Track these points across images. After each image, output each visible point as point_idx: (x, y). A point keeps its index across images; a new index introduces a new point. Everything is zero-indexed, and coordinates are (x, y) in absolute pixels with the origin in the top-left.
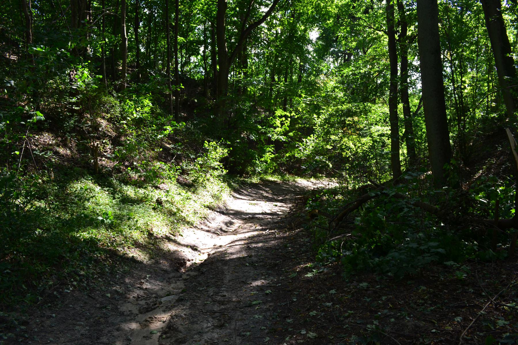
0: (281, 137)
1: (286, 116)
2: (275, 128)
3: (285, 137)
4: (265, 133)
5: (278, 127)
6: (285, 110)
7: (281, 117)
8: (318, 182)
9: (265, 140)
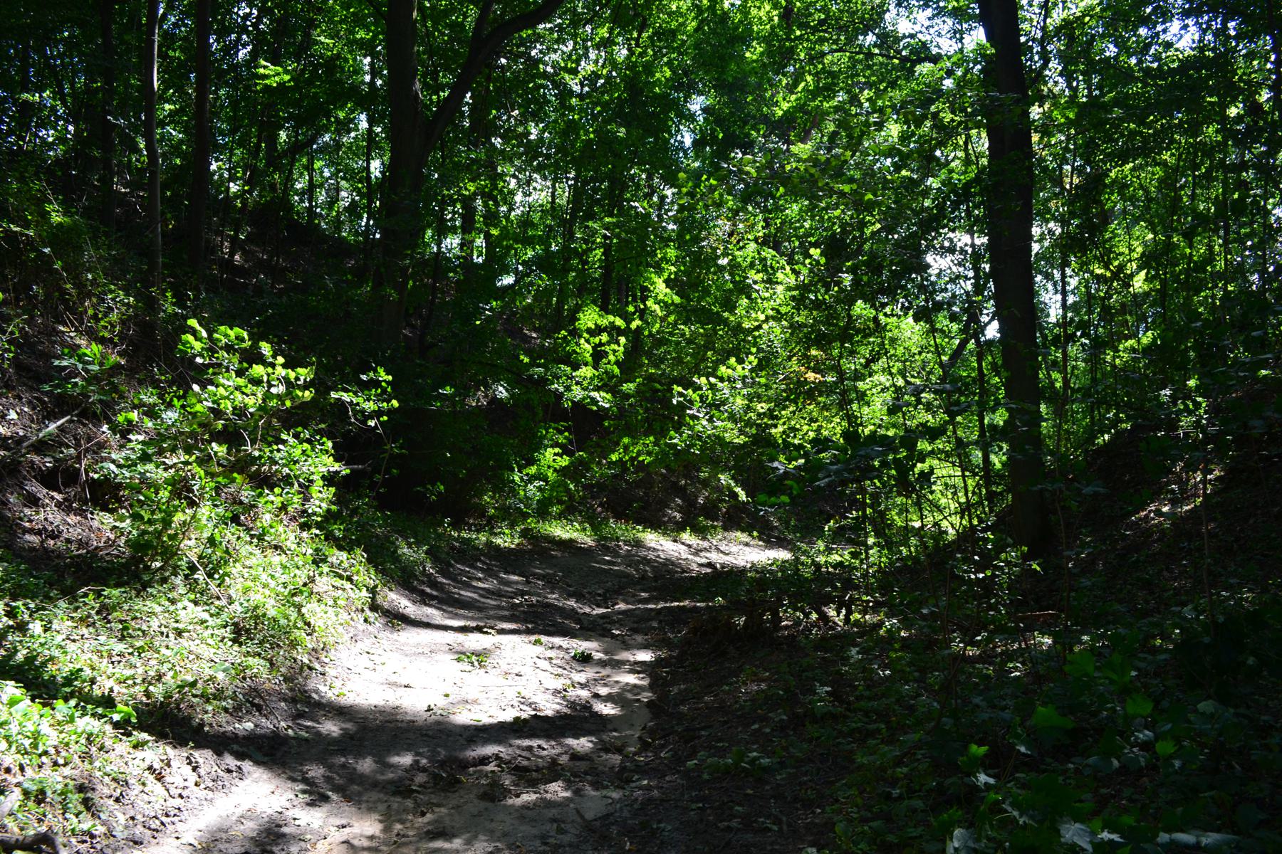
0: (595, 394)
1: (614, 331)
2: (576, 367)
3: (609, 396)
4: (543, 381)
5: (586, 364)
6: (605, 309)
7: (598, 330)
8: (705, 544)
9: (546, 407)
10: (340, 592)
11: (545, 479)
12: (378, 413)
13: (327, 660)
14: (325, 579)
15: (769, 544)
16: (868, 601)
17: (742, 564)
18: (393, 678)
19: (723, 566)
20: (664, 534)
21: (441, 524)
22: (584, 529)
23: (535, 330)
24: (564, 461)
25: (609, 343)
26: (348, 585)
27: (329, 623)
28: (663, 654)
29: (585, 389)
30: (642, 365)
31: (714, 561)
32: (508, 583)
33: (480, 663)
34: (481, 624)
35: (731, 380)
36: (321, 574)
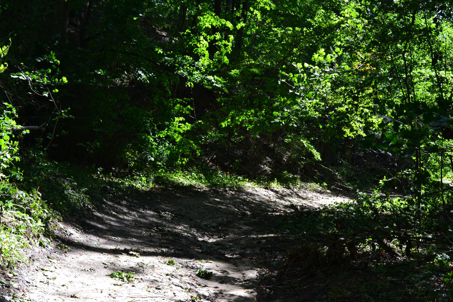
1: (225, 31)
6: (218, 12)
7: (213, 30)
9: (173, 87)
10: (21, 222)
11: (173, 141)
12: (49, 87)
13: (11, 275)
14: (9, 212)
15: (336, 193)
16: (420, 238)
17: (316, 206)
18: (63, 289)
19: (302, 207)
20: (258, 183)
21: (95, 172)
22: (200, 178)
23: (164, 30)
24: (187, 127)
25: (221, 40)
26: (27, 217)
27: (13, 246)
28: (265, 271)
29: (203, 74)
30: (243, 58)
31: (295, 204)
32: (144, 216)
33: (128, 278)
34: (128, 248)
35: (320, 65)
36: (6, 208)
